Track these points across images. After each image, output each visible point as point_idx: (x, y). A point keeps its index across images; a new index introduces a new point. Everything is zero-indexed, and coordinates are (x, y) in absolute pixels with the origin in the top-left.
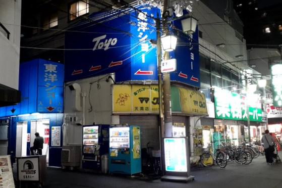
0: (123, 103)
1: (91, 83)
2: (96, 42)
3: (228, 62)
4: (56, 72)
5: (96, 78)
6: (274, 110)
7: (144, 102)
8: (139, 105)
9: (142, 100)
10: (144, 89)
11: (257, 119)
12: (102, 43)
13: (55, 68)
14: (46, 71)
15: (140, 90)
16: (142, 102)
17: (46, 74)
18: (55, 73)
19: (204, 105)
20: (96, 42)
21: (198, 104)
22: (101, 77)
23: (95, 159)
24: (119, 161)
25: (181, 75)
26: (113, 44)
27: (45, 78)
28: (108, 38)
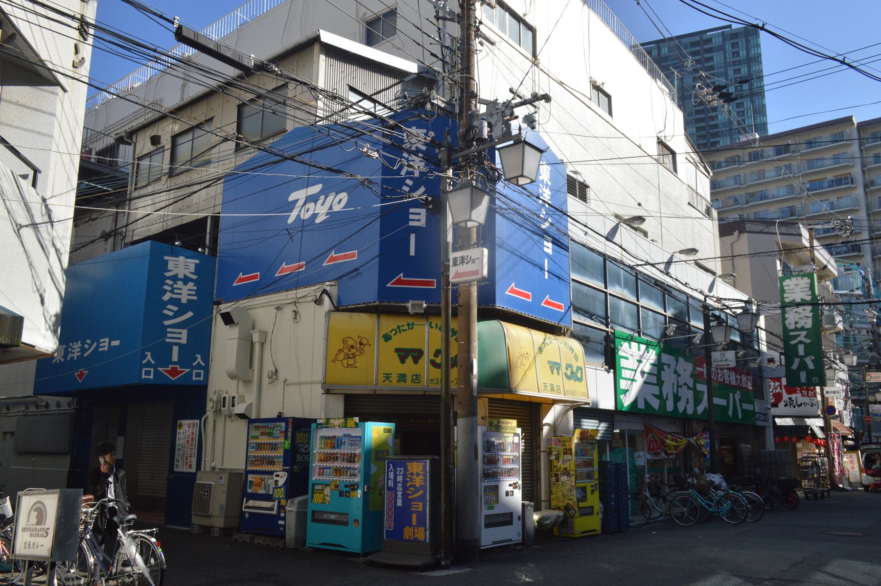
0: (351, 361)
1: (278, 308)
2: (297, 201)
3: (647, 263)
4: (195, 277)
5: (292, 294)
6: (793, 396)
7: (409, 360)
8: (394, 366)
9: (403, 354)
10: (411, 326)
11: (740, 417)
12: (311, 205)
13: (192, 268)
14: (167, 274)
15: (399, 330)
16: (403, 360)
17: (170, 282)
18: (192, 280)
19: (579, 375)
20: (297, 201)
21: (563, 369)
22: (301, 292)
23: (827, 324)
24: (333, 517)
25: (512, 291)
26: (337, 208)
27: (166, 291)
28: (325, 192)
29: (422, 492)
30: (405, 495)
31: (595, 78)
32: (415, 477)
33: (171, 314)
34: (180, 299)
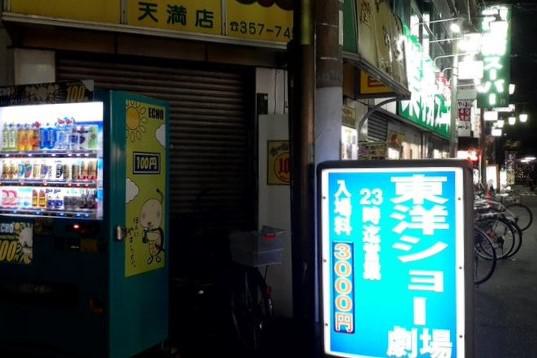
17: (404, 209)
29: (440, 247)
30: (387, 255)
31: (169, 3)
32: (418, 210)
33: (407, 248)
34: (421, 230)
